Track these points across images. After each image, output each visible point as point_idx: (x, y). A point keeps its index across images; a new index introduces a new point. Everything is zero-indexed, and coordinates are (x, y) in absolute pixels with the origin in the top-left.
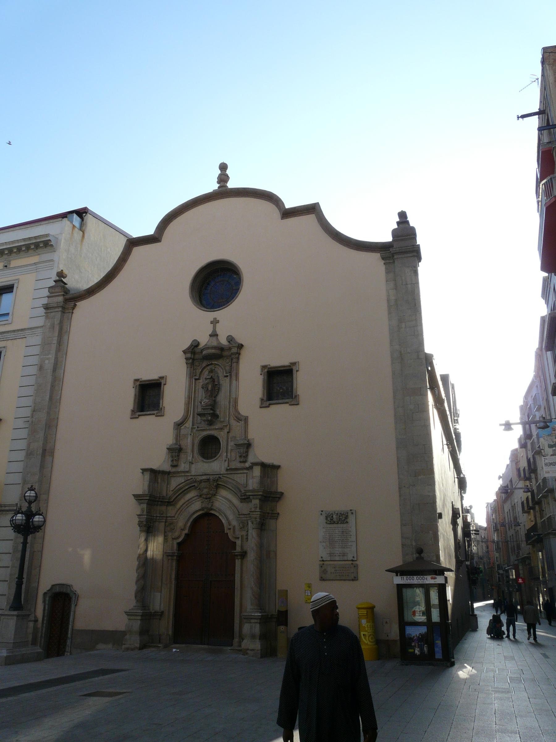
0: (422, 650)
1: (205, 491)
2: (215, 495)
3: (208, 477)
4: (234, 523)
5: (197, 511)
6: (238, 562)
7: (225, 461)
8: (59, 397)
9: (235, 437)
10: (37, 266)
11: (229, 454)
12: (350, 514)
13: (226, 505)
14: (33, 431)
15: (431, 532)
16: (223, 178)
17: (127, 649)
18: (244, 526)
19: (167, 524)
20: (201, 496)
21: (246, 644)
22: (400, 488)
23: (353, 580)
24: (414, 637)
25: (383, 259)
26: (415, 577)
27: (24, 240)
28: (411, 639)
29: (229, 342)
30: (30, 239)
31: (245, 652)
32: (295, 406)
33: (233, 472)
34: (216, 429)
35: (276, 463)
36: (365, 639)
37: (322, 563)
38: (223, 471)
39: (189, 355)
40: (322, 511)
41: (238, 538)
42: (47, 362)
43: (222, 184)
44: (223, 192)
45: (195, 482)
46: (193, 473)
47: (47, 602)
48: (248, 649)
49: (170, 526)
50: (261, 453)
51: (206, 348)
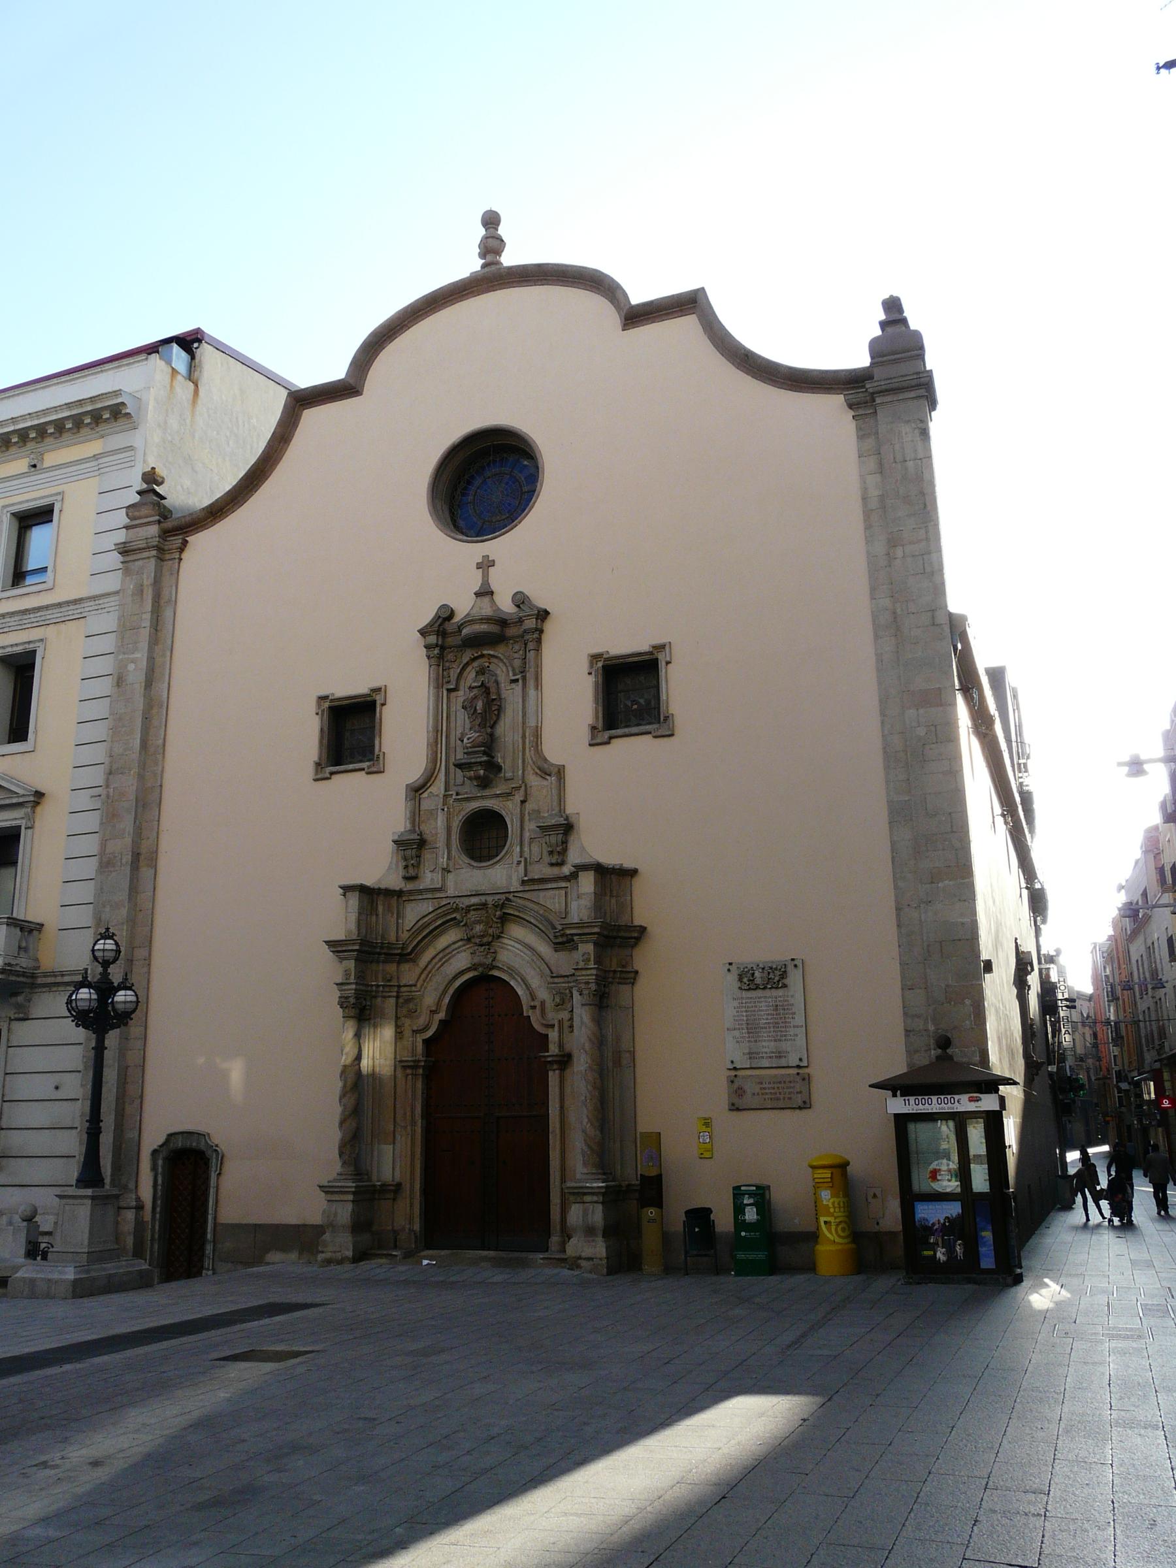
0: (950, 1251)
1: (478, 928)
2: (499, 937)
3: (483, 898)
4: (543, 994)
5: (462, 973)
6: (553, 1077)
7: (519, 863)
8: (161, 741)
9: (539, 812)
10: (100, 461)
11: (526, 849)
12: (790, 968)
13: (524, 957)
14: (110, 816)
15: (968, 1002)
16: (491, 246)
17: (329, 1262)
18: (564, 999)
19: (401, 1000)
20: (469, 940)
21: (576, 1246)
22: (898, 909)
23: (800, 1108)
24: (933, 1224)
25: (851, 406)
26: (934, 1098)
27: (69, 405)
28: (928, 1230)
30: (80, 402)
31: (574, 1263)
32: (666, 739)
33: (532, 887)
34: (498, 796)
35: (628, 864)
36: (830, 1232)
37: (733, 1073)
38: (515, 885)
39: (432, 639)
41: (553, 1026)
42: (131, 667)
43: (489, 258)
44: (494, 277)
45: (456, 910)
46: (451, 891)
47: (160, 1170)
48: (580, 1258)
49: (406, 1004)
50: (596, 843)
51: (469, 621)
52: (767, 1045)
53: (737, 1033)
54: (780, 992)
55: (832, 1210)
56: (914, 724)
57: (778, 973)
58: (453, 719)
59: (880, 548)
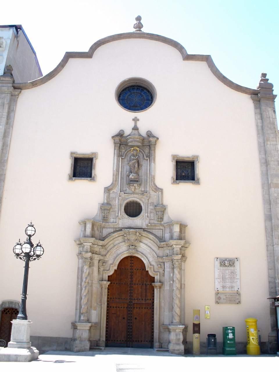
4: (153, 263)
13: (147, 252)
16: (139, 26)
29: (148, 136)
40: (217, 258)
44: (139, 34)
48: (174, 350)
52: (228, 284)
55: (254, 335)
56: (274, 192)
58: (123, 168)
59: (261, 140)
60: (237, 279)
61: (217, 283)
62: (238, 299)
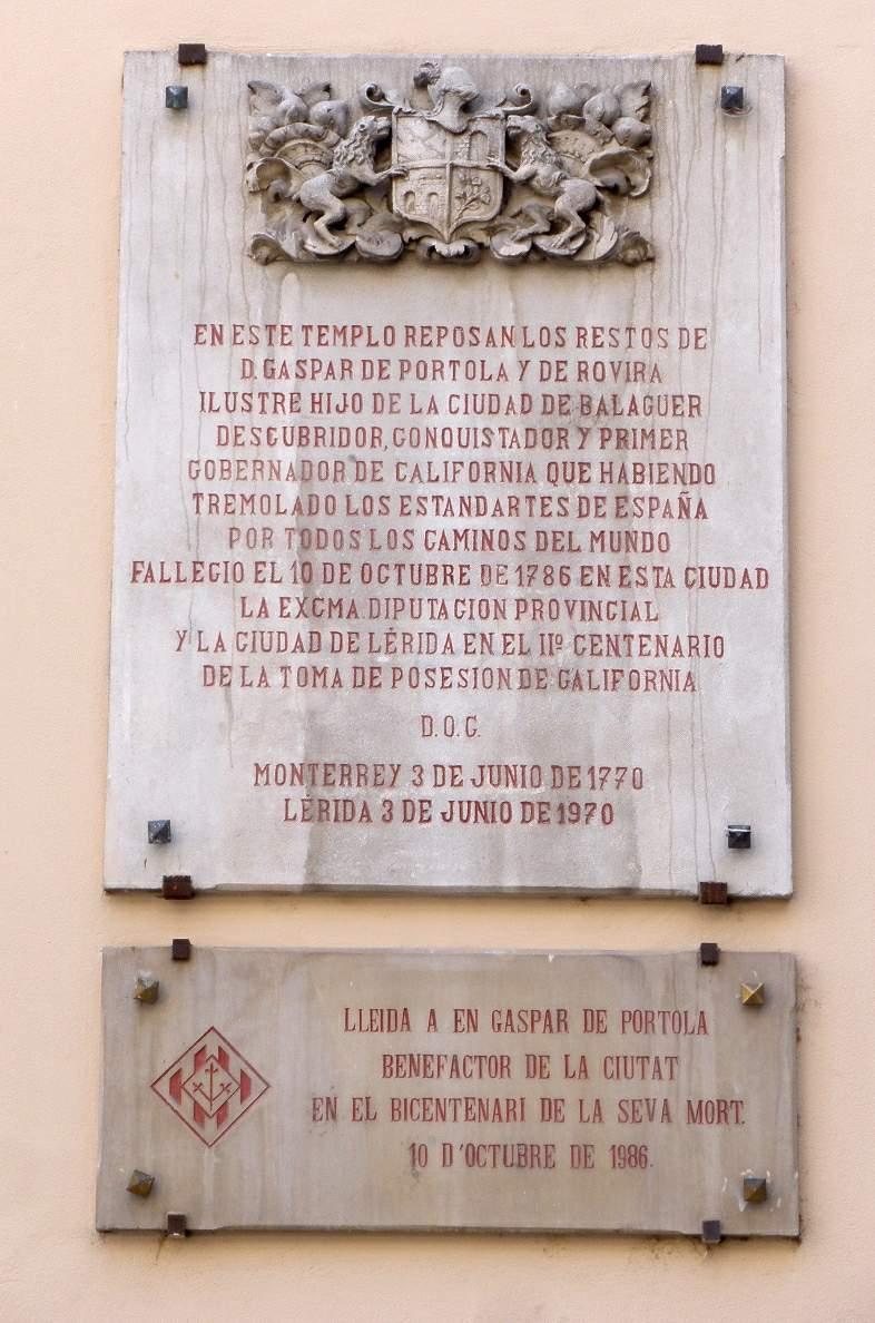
10: (121, 396)
12: (686, 112)
23: (714, 1238)
37: (159, 928)
52: (458, 717)
53: (212, 610)
54: (591, 303)
57: (584, 147)
60: (698, 578)
61: (152, 683)
62: (724, 1110)
